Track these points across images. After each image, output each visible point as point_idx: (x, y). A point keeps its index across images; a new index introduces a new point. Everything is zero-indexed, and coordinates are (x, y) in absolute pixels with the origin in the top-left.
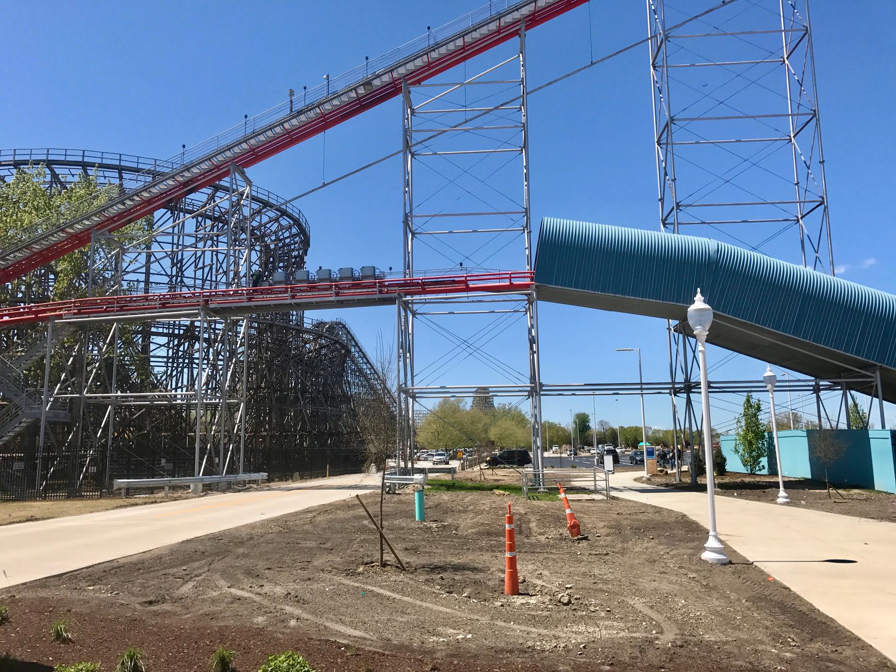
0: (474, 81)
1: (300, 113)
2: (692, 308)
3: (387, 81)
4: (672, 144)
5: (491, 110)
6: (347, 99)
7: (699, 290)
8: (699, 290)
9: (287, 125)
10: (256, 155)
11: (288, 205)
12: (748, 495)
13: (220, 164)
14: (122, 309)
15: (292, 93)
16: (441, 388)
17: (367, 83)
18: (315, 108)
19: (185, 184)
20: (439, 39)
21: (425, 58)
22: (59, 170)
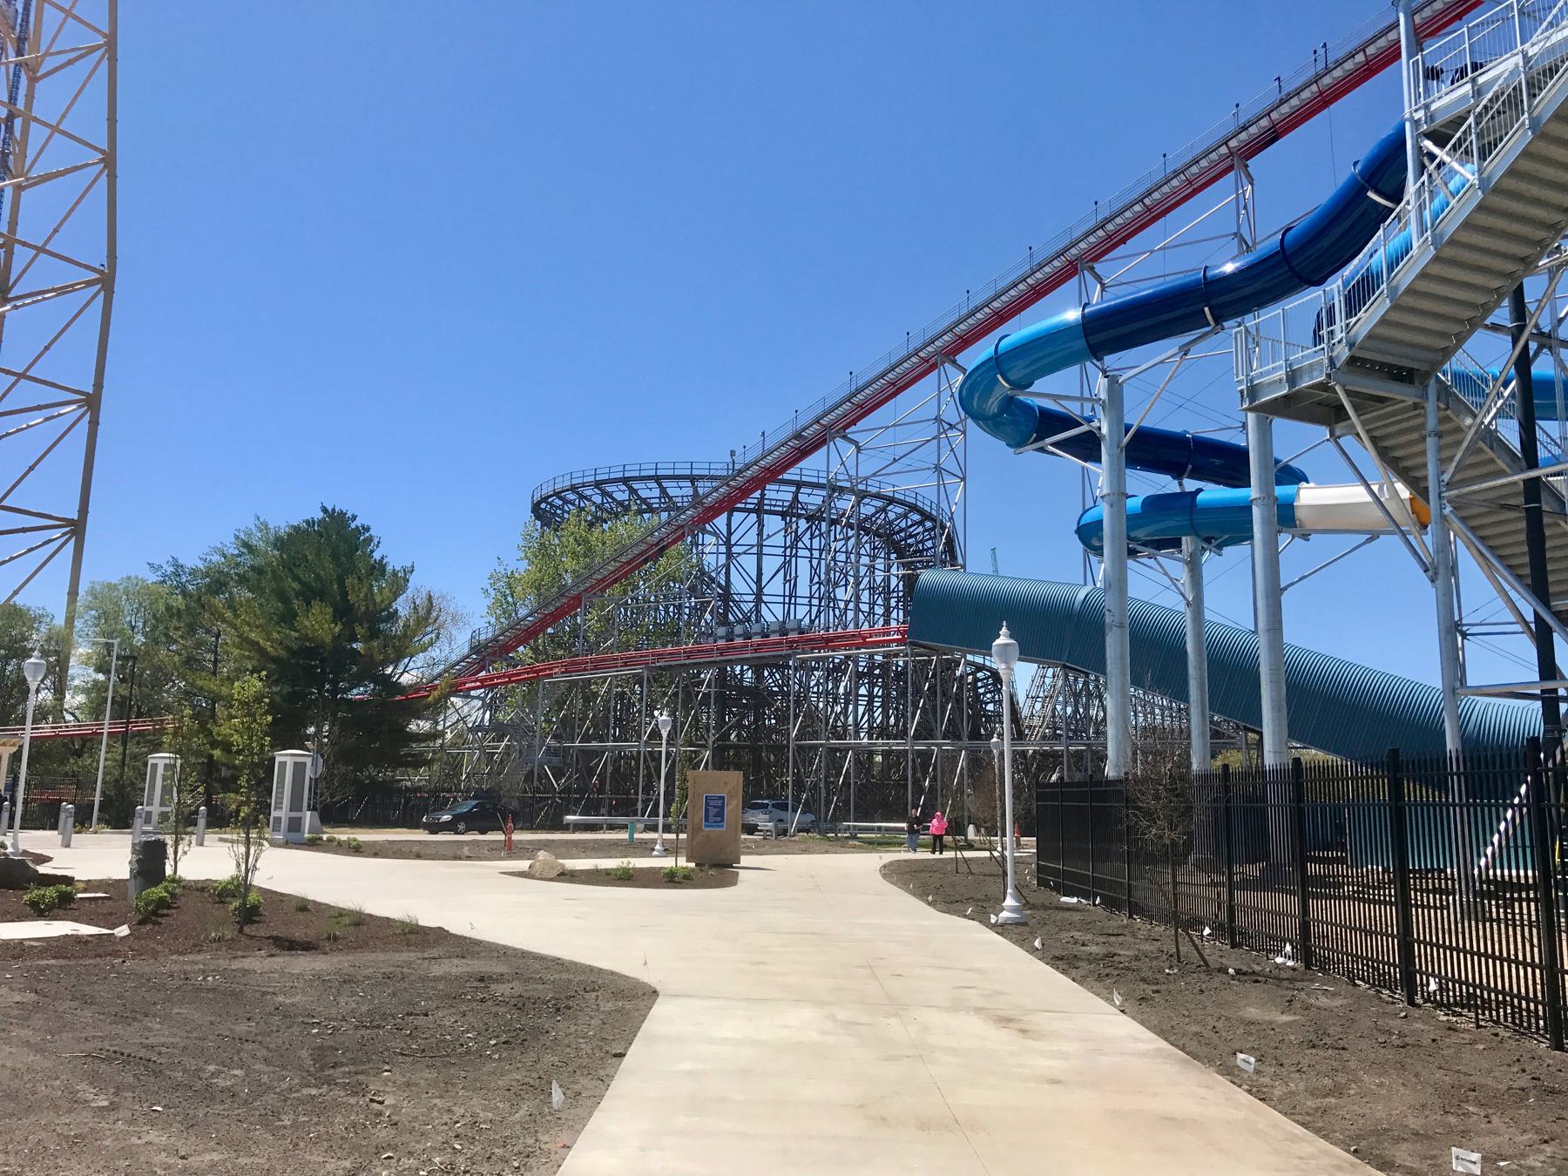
0: (1174, 243)
1: (1339, 64)
2: (997, 642)
3: (1265, 127)
4: (1286, 343)
5: (928, 441)
6: (1059, 264)
7: (1004, 623)
8: (1004, 623)
9: (1030, 281)
10: (803, 453)
11: (870, 482)
12: (1279, 711)
13: (861, 403)
14: (626, 664)
15: (733, 453)
16: (684, 790)
17: (798, 436)
18: (1178, 175)
19: (629, 563)
20: (860, 383)
21: (1314, 88)
22: (610, 488)
